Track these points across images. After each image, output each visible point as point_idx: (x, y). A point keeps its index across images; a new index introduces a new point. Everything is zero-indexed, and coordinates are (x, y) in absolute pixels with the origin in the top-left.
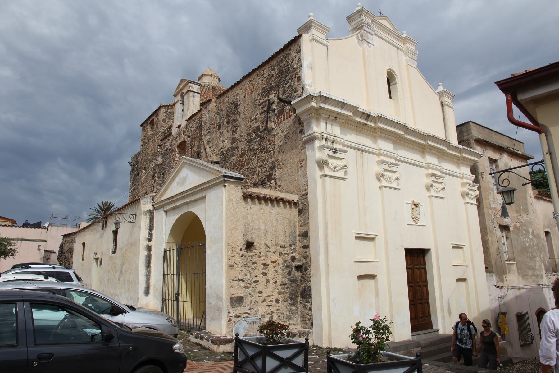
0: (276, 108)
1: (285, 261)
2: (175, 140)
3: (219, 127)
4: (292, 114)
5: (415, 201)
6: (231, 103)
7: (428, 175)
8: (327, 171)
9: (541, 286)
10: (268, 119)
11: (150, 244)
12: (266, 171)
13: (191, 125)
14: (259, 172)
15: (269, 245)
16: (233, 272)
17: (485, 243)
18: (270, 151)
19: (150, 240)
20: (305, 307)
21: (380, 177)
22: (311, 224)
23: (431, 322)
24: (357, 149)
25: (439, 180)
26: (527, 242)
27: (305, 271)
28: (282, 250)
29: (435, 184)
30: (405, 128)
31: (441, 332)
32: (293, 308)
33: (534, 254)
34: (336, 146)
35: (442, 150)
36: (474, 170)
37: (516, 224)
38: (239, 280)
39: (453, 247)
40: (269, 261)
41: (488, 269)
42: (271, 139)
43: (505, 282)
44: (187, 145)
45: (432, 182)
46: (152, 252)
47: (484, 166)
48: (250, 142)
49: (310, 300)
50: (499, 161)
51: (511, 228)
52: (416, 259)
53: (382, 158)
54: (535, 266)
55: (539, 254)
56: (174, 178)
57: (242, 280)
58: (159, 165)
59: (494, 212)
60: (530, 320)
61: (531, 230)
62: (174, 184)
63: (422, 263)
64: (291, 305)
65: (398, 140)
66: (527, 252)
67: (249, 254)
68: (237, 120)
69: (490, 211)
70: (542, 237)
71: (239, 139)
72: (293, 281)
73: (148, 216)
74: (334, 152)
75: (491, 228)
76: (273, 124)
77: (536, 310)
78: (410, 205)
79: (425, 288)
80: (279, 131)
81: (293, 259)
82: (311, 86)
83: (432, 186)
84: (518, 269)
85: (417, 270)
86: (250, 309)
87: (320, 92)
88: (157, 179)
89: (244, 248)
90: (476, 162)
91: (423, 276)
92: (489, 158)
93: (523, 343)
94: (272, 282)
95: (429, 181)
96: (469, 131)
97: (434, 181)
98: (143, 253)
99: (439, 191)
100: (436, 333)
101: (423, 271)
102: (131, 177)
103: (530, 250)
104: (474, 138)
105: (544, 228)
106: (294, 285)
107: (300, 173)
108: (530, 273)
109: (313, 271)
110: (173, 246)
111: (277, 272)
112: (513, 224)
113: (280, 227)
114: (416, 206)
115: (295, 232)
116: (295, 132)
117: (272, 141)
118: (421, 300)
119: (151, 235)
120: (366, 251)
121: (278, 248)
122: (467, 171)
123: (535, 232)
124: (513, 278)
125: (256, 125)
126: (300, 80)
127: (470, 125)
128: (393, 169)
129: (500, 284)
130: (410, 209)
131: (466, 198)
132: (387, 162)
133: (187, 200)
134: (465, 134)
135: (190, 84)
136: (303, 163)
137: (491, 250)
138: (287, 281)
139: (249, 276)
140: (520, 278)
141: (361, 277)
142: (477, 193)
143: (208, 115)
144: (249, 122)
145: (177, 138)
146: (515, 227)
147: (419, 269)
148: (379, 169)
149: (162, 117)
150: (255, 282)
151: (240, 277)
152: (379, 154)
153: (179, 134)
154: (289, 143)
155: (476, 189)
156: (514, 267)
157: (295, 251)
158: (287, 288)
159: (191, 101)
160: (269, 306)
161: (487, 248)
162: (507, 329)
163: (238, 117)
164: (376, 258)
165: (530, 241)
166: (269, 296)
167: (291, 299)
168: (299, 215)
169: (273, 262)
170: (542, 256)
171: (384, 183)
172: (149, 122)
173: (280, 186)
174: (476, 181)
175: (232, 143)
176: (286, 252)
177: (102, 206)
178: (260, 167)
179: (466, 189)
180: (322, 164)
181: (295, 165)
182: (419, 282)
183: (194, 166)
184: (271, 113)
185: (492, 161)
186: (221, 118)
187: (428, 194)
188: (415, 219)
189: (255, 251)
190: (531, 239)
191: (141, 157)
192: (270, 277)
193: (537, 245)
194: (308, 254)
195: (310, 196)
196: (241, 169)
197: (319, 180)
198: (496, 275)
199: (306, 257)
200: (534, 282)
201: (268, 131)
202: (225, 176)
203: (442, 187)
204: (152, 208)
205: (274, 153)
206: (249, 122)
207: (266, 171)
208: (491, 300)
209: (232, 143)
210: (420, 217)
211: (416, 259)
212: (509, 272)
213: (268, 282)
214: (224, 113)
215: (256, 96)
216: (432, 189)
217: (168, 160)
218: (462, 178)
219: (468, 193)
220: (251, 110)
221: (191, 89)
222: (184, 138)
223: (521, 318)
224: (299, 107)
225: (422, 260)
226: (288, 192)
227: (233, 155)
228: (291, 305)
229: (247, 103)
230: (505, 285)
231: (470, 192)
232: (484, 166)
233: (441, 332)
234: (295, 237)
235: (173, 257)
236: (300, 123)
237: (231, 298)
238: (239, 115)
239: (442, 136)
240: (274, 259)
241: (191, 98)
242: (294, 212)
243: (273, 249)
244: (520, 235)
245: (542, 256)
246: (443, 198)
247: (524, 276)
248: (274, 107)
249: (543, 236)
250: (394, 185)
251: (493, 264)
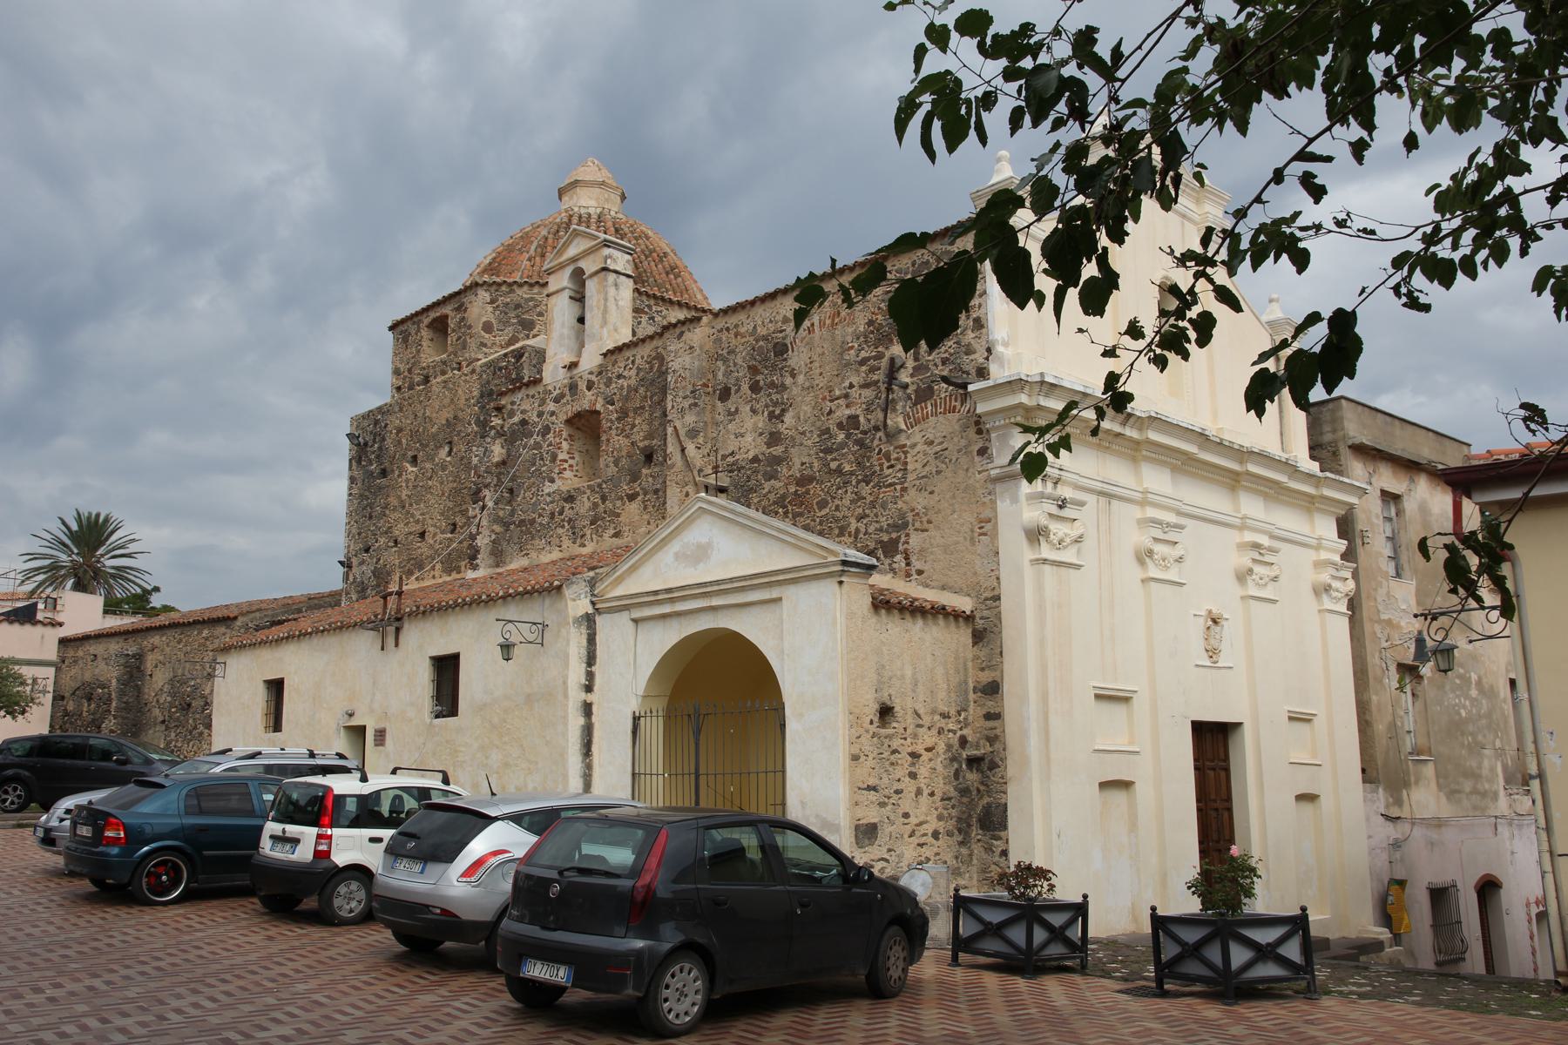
0: (908, 380)
1: (949, 747)
2: (557, 400)
3: (725, 394)
4: (958, 404)
6: (765, 338)
7: (1243, 546)
8: (1046, 552)
10: (888, 407)
11: (590, 698)
12: (881, 530)
13: (618, 370)
14: (857, 530)
15: (921, 712)
16: (858, 771)
17: (1363, 708)
18: (891, 485)
19: (589, 688)
20: (989, 849)
21: (1143, 556)
22: (1006, 667)
24: (1101, 493)
25: (1267, 558)
26: (1464, 707)
27: (990, 769)
28: (942, 723)
29: (1258, 569)
30: (1202, 438)
32: (964, 851)
33: (1480, 738)
34: (1065, 492)
36: (1346, 527)
38: (869, 788)
39: (1291, 718)
40: (920, 749)
42: (894, 456)
43: (1406, 807)
44: (605, 424)
45: (1250, 564)
46: (594, 719)
47: (1370, 511)
48: (828, 451)
49: (1002, 834)
50: (1405, 498)
52: (1213, 741)
53: (1151, 512)
54: (1480, 767)
55: (1491, 737)
56: (665, 542)
57: (874, 789)
58: (498, 465)
60: (1462, 902)
61: (1474, 677)
62: (667, 556)
63: (1222, 755)
64: (961, 843)
65: (1183, 465)
66: (1463, 734)
67: (883, 731)
68: (784, 387)
69: (1377, 628)
70: (1502, 695)
71: (793, 438)
72: (964, 791)
73: (584, 630)
74: (1061, 507)
76: (900, 419)
78: (1202, 620)
80: (917, 438)
81: (963, 741)
82: (1006, 345)
83: (1250, 571)
84: (1438, 776)
85: (1211, 773)
86: (889, 850)
87: (1042, 374)
88: (490, 504)
89: (876, 719)
90: (1351, 507)
91: (1224, 788)
93: (1441, 958)
94: (926, 793)
95: (1245, 561)
96: (1336, 422)
97: (1254, 560)
98: (576, 722)
101: (1223, 774)
102: (352, 480)
103: (1471, 728)
105: (1508, 671)
106: (965, 800)
107: (979, 548)
108: (1467, 786)
109: (1011, 770)
110: (659, 705)
111: (935, 773)
113: (940, 671)
114: (1215, 621)
115: (966, 682)
116: (964, 451)
117: (898, 459)
119: (590, 676)
120: (1112, 730)
121: (937, 717)
122: (1327, 529)
125: (848, 412)
126: (982, 327)
127: (1340, 408)
128: (1171, 536)
129: (1395, 812)
130: (1202, 628)
131: (1324, 596)
132: (1160, 523)
133: (715, 602)
134: (1327, 428)
135: (607, 251)
136: (988, 527)
138: (953, 793)
139: (885, 780)
140: (1444, 799)
141: (1104, 785)
142: (1351, 585)
143: (688, 359)
144: (824, 399)
145: (562, 396)
148: (1143, 539)
149: (480, 316)
150: (898, 792)
151: (872, 782)
152: (1143, 503)
153: (573, 387)
154: (948, 473)
155: (1349, 575)
156: (1429, 771)
157: (966, 725)
158: (953, 807)
159: (611, 300)
160: (921, 845)
162: (1406, 922)
163: (788, 381)
164: (1131, 743)
166: (920, 824)
167: (960, 831)
168: (975, 644)
169: (928, 750)
170: (1498, 744)
171: (1154, 572)
172: (427, 321)
173: (920, 572)
174: (1348, 555)
175: (769, 445)
176: (951, 726)
177: (75, 527)
178: (860, 518)
179: (1325, 577)
180: (1036, 535)
181: (966, 528)
183: (738, 523)
184: (898, 393)
185: (1390, 498)
186: (728, 373)
187: (1240, 592)
188: (1212, 653)
189: (896, 726)
191: (394, 421)
192: (922, 782)
193: (1489, 715)
194: (998, 732)
195: (1006, 604)
196: (801, 515)
197: (1029, 572)
199: (992, 740)
201: (887, 435)
202: (844, 563)
203: (1273, 574)
204: (590, 610)
205: (904, 489)
206: (824, 399)
207: (881, 530)
208: (1372, 850)
209: (769, 445)
210: (1222, 647)
211: (1213, 741)
212: (1417, 782)
213: (919, 792)
214: (739, 361)
215: (849, 339)
216: (1250, 582)
217: (525, 454)
218: (1318, 548)
220: (830, 369)
221: (611, 265)
222: (587, 400)
223: (1440, 896)
224: (984, 400)
226: (943, 588)
227: (771, 476)
228: (961, 843)
229: (819, 350)
230: (1405, 813)
232: (1370, 511)
234: (966, 692)
235: (654, 730)
236: (979, 432)
237: (857, 827)
238: (793, 376)
239: (1274, 450)
240: (929, 742)
241: (612, 291)
242: (964, 635)
243: (927, 720)
244: (1448, 687)
245: (1498, 744)
247: (1453, 794)
248: (904, 377)
249: (1504, 690)
250: (1172, 575)
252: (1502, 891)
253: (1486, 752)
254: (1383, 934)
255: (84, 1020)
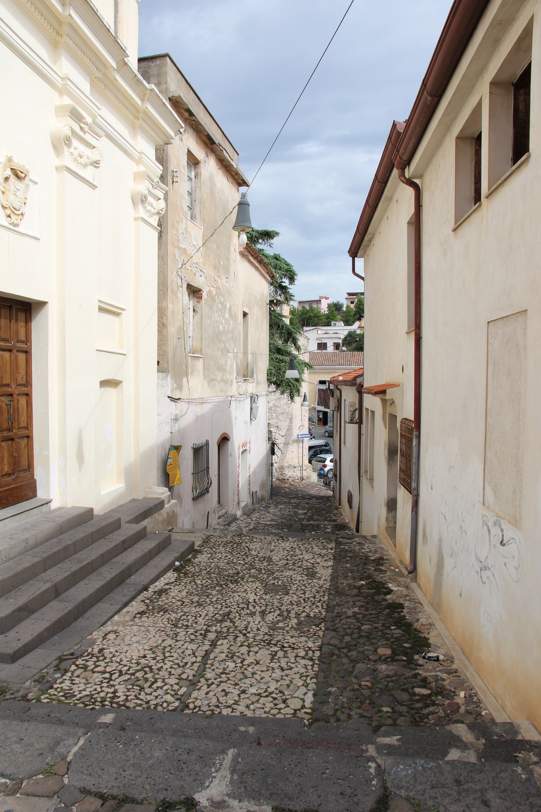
5: (15, 160)
9: (230, 398)
17: (162, 312)
23: (35, 482)
25: (88, 137)
26: (222, 324)
31: (54, 505)
35: (104, 65)
37: (212, 289)
39: (101, 309)
41: (162, 366)
50: (202, 165)
51: (204, 295)
54: (226, 365)
59: (183, 258)
61: (228, 305)
75: (175, 287)
77: (219, 437)
79: (23, 401)
91: (22, 371)
92: (189, 152)
99: (85, 166)
100: (44, 508)
101: (22, 357)
104: (170, 95)
112: (208, 289)
118: (9, 430)
123: (233, 309)
124: (196, 385)
127: (165, 64)
137: (169, 328)
142: (162, 204)
146: (209, 293)
147: (10, 351)
155: (162, 196)
161: (163, 324)
165: (225, 322)
179: (143, 187)
182: (8, 385)
190: (227, 320)
198: (172, 378)
200: (222, 391)
212: (192, 373)
219: (146, 197)
225: (22, 331)
231: (150, 199)
233: (54, 505)
244: (215, 309)
246: (93, 187)
247: (211, 381)
251: (170, 356)
252: (230, 442)
253: (230, 354)
254: (162, 492)
255: (145, 669)
